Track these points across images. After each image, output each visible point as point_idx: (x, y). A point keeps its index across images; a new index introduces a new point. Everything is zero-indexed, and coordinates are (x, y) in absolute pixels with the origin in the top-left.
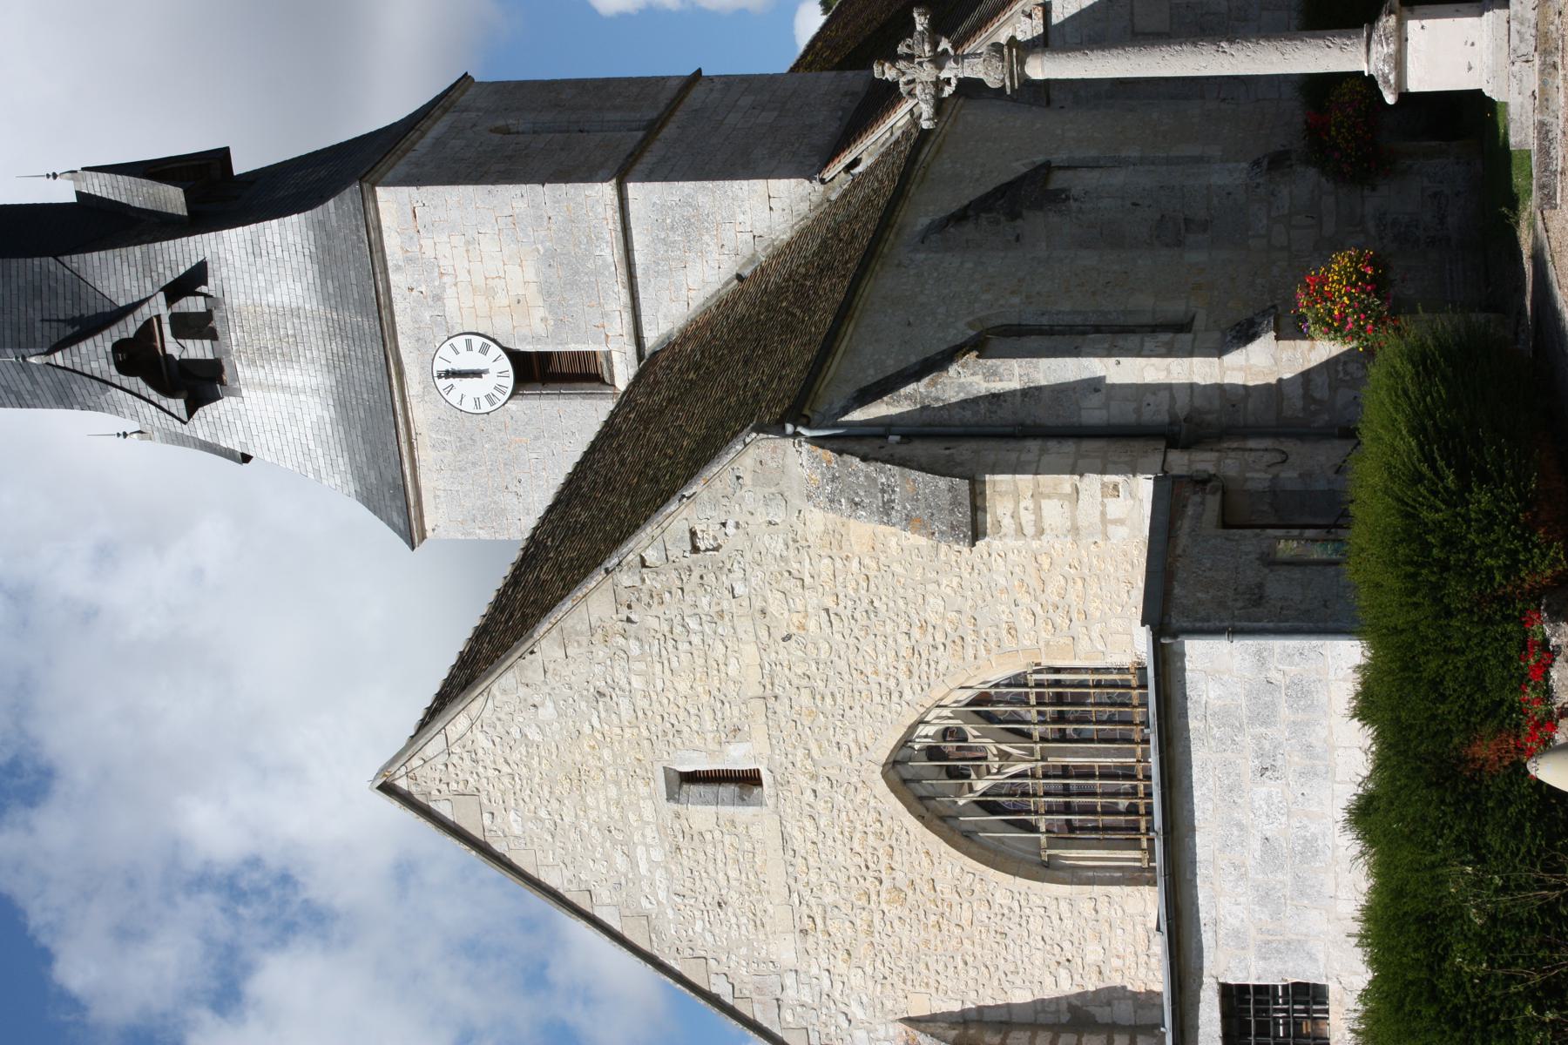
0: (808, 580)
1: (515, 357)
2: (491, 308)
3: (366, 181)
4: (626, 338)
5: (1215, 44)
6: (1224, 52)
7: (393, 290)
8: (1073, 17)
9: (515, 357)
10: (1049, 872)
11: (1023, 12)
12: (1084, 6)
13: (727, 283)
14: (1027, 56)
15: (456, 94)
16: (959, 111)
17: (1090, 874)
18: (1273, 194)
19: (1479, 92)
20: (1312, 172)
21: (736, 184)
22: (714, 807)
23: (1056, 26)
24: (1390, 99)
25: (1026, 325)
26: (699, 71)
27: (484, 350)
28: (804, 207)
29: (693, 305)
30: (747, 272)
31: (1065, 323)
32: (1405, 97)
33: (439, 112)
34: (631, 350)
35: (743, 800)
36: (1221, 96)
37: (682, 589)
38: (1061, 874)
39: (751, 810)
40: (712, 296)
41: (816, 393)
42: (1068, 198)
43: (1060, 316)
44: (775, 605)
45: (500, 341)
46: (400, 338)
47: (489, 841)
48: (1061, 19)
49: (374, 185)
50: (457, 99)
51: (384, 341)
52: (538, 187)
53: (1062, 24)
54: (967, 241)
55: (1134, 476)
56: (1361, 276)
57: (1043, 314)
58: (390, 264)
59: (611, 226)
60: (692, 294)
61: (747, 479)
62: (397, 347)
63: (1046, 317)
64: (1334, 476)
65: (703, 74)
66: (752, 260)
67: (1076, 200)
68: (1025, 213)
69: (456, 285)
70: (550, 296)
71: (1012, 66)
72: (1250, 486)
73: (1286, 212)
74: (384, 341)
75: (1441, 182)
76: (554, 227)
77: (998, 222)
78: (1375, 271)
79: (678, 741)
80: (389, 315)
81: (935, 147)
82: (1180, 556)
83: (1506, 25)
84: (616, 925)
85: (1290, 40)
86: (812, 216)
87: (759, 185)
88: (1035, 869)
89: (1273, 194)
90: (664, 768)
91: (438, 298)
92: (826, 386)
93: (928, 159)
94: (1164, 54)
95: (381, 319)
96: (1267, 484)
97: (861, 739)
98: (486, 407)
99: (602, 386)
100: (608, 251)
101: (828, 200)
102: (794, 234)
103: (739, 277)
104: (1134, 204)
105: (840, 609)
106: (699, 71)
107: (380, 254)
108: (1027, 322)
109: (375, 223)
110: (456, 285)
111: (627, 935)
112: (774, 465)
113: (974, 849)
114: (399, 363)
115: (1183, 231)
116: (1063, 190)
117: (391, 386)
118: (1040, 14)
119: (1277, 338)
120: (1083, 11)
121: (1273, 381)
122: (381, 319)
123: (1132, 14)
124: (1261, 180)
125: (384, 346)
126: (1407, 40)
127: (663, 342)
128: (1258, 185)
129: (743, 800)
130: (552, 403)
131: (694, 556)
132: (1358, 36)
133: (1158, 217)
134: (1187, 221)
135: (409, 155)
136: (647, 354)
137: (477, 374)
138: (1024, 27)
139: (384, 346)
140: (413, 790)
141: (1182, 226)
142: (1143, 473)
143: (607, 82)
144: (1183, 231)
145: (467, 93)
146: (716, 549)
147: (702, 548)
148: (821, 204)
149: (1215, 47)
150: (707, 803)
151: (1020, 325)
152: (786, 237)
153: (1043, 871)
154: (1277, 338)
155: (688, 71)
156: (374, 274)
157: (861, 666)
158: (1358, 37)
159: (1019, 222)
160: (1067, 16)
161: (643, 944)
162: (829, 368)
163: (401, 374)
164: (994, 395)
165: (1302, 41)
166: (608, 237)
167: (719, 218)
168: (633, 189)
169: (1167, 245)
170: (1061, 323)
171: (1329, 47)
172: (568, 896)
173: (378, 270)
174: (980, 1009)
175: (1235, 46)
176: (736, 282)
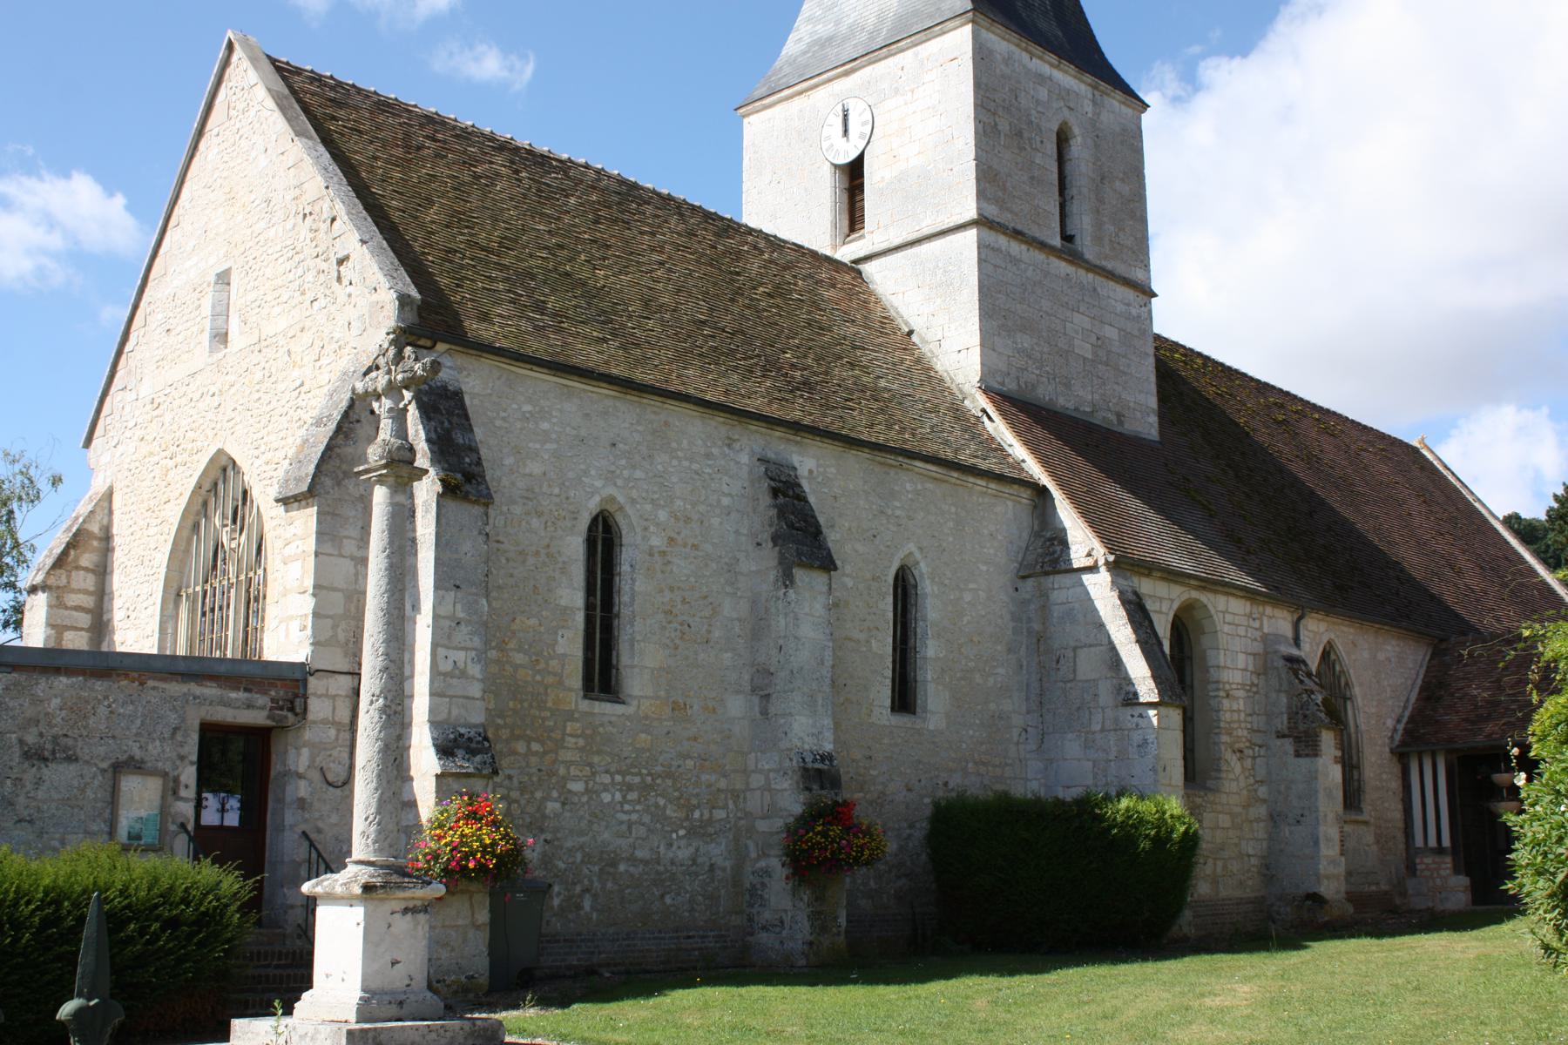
0: (318, 364)
1: (860, 160)
2: (890, 135)
3: (974, 14)
4: (871, 248)
5: (381, 692)
6: (372, 702)
7: (901, 55)
8: (1088, 593)
9: (860, 160)
10: (173, 597)
11: (1093, 549)
12: (1096, 602)
13: (906, 323)
14: (388, 487)
15: (1118, 97)
16: (1010, 500)
17: (170, 631)
18: (785, 773)
19: (308, 984)
20: (798, 809)
21: (977, 319)
22: (209, 313)
23: (1081, 579)
24: (306, 888)
25: (621, 552)
26: (1155, 295)
27: (862, 136)
28: (960, 379)
29: (892, 298)
30: (915, 338)
31: (622, 586)
32: (311, 903)
33: (1089, 81)
34: (862, 254)
35: (215, 337)
36: (1029, 729)
37: (317, 256)
38: (171, 606)
39: (207, 343)
40: (898, 313)
41: (480, 356)
42: (786, 586)
43: (630, 582)
44: (306, 338)
45: (869, 146)
46: (870, 68)
47: (206, 135)
48: (1086, 583)
49: (973, 21)
50: (1114, 98)
51: (866, 54)
52: (973, 156)
53: (1082, 585)
54: (758, 499)
55: (312, 644)
56: (466, 857)
57: (632, 566)
58: (919, 48)
59: (947, 221)
60: (901, 296)
61: (375, 297)
62: (864, 66)
63: (629, 569)
64: (300, 831)
65: (1153, 300)
66: (925, 342)
67: (785, 594)
68: (777, 548)
69: (906, 104)
70: (899, 181)
71: (375, 470)
72: (292, 752)
73: (773, 786)
74: (866, 54)
75: (791, 928)
76: (945, 174)
77: (771, 526)
78: (473, 870)
79: (242, 275)
80: (883, 55)
81: (939, 476)
82: (142, 684)
83: (344, 1020)
84: (162, 251)
85: (379, 776)
86: (953, 387)
87: (976, 339)
88: (175, 586)
89: (785, 773)
90: (230, 268)
91: (897, 91)
92: (498, 367)
93: (916, 469)
94: (375, 637)
95: (881, 48)
96: (293, 768)
97: (237, 428)
98: (825, 145)
99: (843, 236)
100: (930, 222)
101: (964, 399)
102: (940, 373)
103: (911, 333)
104: (781, 647)
105: (303, 395)
106: (1155, 295)
107: (924, 38)
108: (624, 553)
109: (945, 29)
110: (906, 104)
111: (158, 261)
112: (380, 319)
113: (185, 533)
114: (853, 71)
115: (761, 693)
116: (792, 582)
117: (836, 67)
118: (1088, 564)
119: (437, 775)
120: (1092, 601)
121: (413, 773)
122: (881, 48)
123: (1090, 646)
124: (794, 763)
125: (863, 56)
126: (351, 906)
127: (868, 278)
128: (791, 760)
129: (215, 337)
130: (828, 197)
131: (335, 262)
132: (378, 851)
133: (772, 670)
134: (768, 695)
135: (1024, 54)
136: (860, 267)
137: (846, 132)
138: (1081, 550)
139: (863, 56)
140: (232, 67)
141: (766, 692)
142: (313, 652)
143: (1142, 220)
144: (761, 693)
145: (1123, 107)
146: (339, 279)
147: (342, 268)
148: (961, 391)
149: (377, 692)
150: (213, 307)
151: (621, 545)
152: (938, 367)
153: (173, 592)
154: (437, 775)
155: (1155, 287)
156: (910, 36)
157: (273, 420)
158: (375, 851)
159: (770, 544)
160: (1089, 588)
161: (152, 276)
162: (531, 370)
163: (847, 74)
164: (414, 512)
165: (377, 789)
166: (939, 220)
167: (952, 309)
168: (972, 234)
169: (752, 679)
170: (623, 582)
171: (366, 819)
172: (177, 208)
173: (913, 38)
174: (113, 550)
175: (377, 716)
176: (907, 330)
